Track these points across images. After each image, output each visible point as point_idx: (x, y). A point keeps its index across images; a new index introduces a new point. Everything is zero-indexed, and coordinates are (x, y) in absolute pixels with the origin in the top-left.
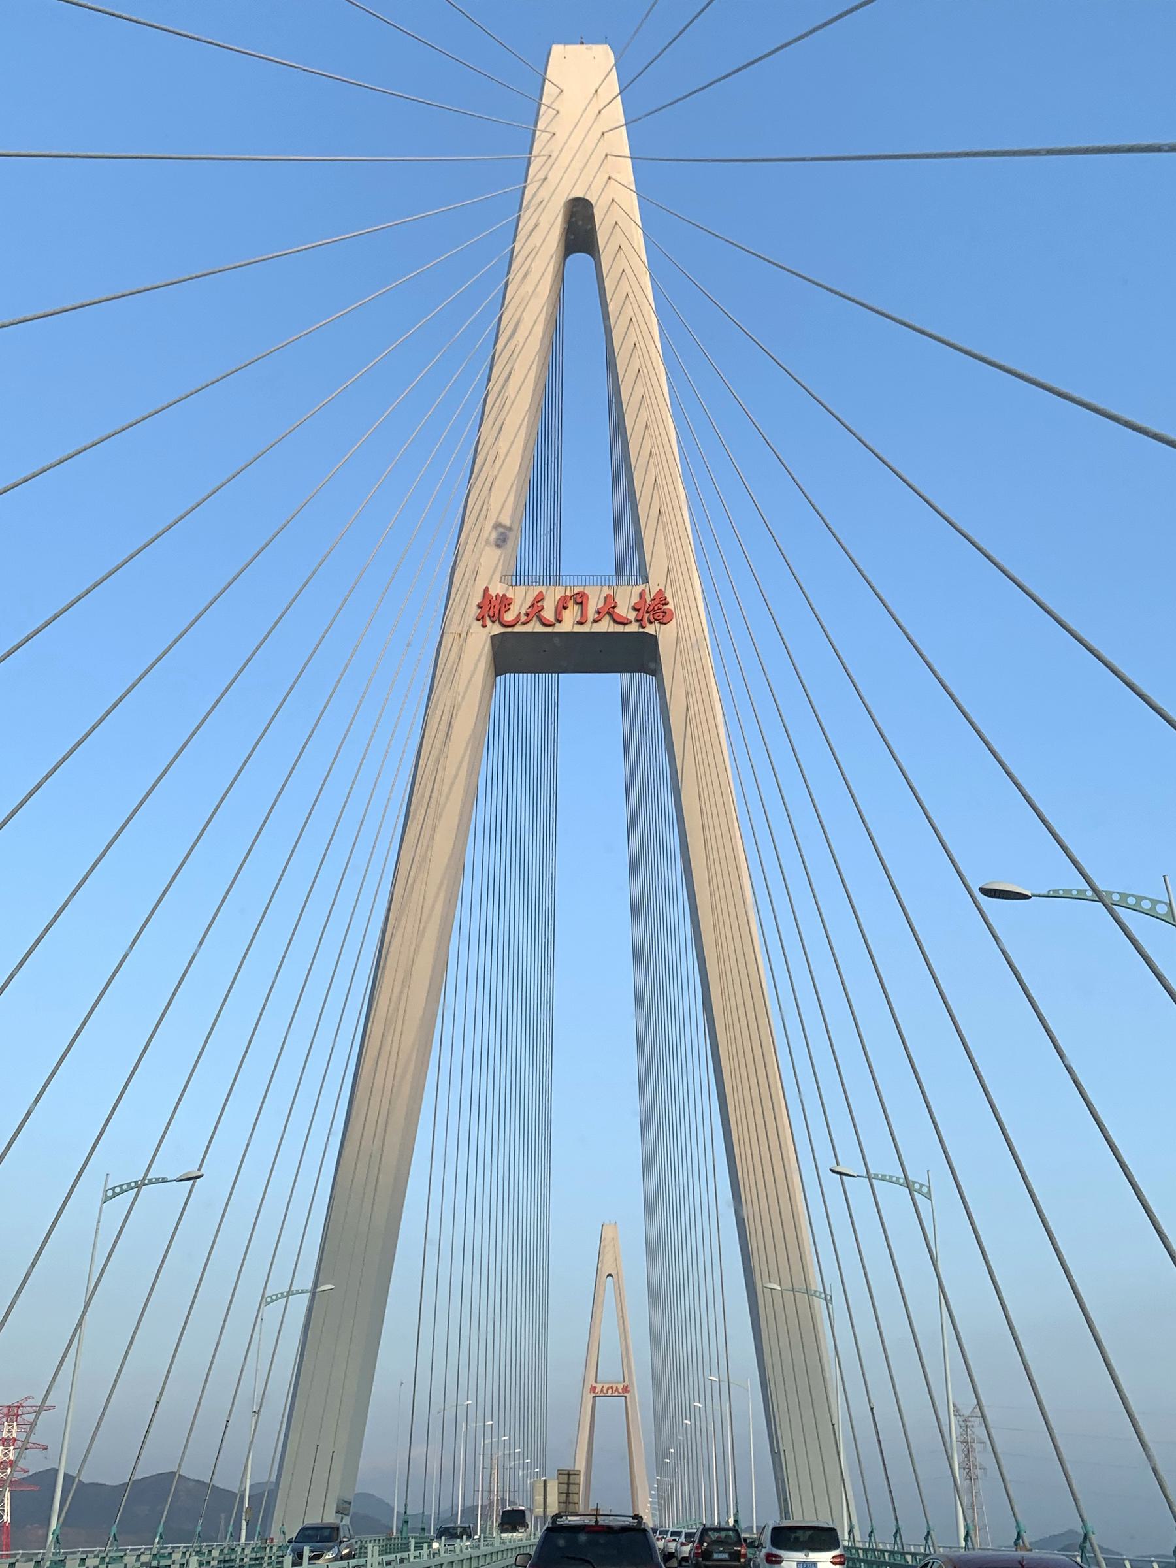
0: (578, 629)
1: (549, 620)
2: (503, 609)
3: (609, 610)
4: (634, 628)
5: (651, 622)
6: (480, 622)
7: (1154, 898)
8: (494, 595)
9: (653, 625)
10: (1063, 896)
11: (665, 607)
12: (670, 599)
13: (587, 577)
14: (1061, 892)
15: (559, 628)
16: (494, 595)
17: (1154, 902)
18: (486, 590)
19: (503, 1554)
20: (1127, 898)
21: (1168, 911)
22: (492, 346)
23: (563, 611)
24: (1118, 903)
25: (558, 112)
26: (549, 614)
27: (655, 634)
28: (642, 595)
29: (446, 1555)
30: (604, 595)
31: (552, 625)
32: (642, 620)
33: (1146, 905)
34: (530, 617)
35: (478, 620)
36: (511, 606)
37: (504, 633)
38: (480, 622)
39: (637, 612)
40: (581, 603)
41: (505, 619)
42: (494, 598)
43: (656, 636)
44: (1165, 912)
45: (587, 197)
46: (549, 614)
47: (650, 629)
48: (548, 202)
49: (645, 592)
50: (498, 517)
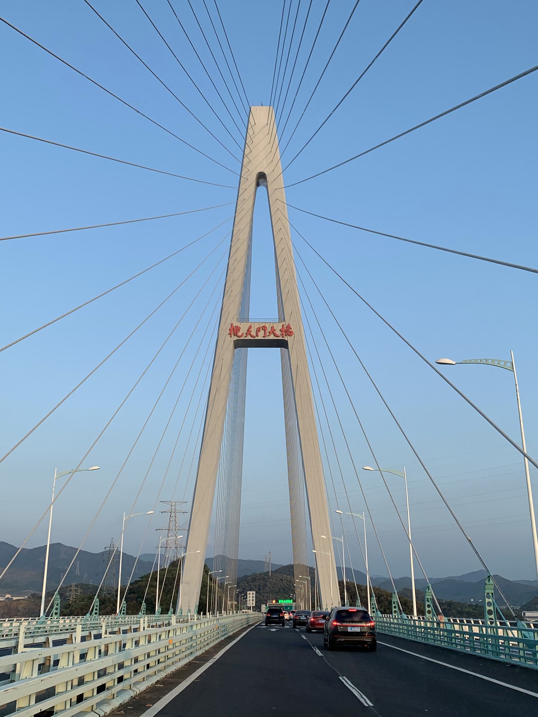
0: (264, 338)
1: (253, 336)
2: (238, 331)
3: (273, 331)
4: (281, 338)
5: (286, 336)
6: (230, 335)
7: (506, 360)
8: (234, 326)
9: (287, 337)
10: (474, 362)
11: (290, 330)
12: (292, 327)
13: (266, 319)
14: (473, 361)
15: (256, 338)
16: (234, 326)
17: (506, 362)
18: (232, 324)
19: (219, 620)
20: (495, 361)
21: (511, 366)
22: (230, 262)
23: (259, 332)
24: (491, 364)
25: (249, 170)
26: (253, 333)
27: (287, 340)
28: (283, 326)
29: (212, 618)
30: (271, 326)
31: (255, 337)
32: (283, 335)
33: (502, 364)
34: (247, 334)
35: (229, 335)
36: (240, 330)
37: (238, 340)
38: (230, 335)
39: (281, 332)
40: (264, 330)
41: (238, 334)
42: (235, 327)
43: (287, 341)
44: (509, 366)
45: (264, 172)
46: (253, 333)
47: (286, 338)
48: (247, 200)
49: (284, 325)
50: (248, 176)
